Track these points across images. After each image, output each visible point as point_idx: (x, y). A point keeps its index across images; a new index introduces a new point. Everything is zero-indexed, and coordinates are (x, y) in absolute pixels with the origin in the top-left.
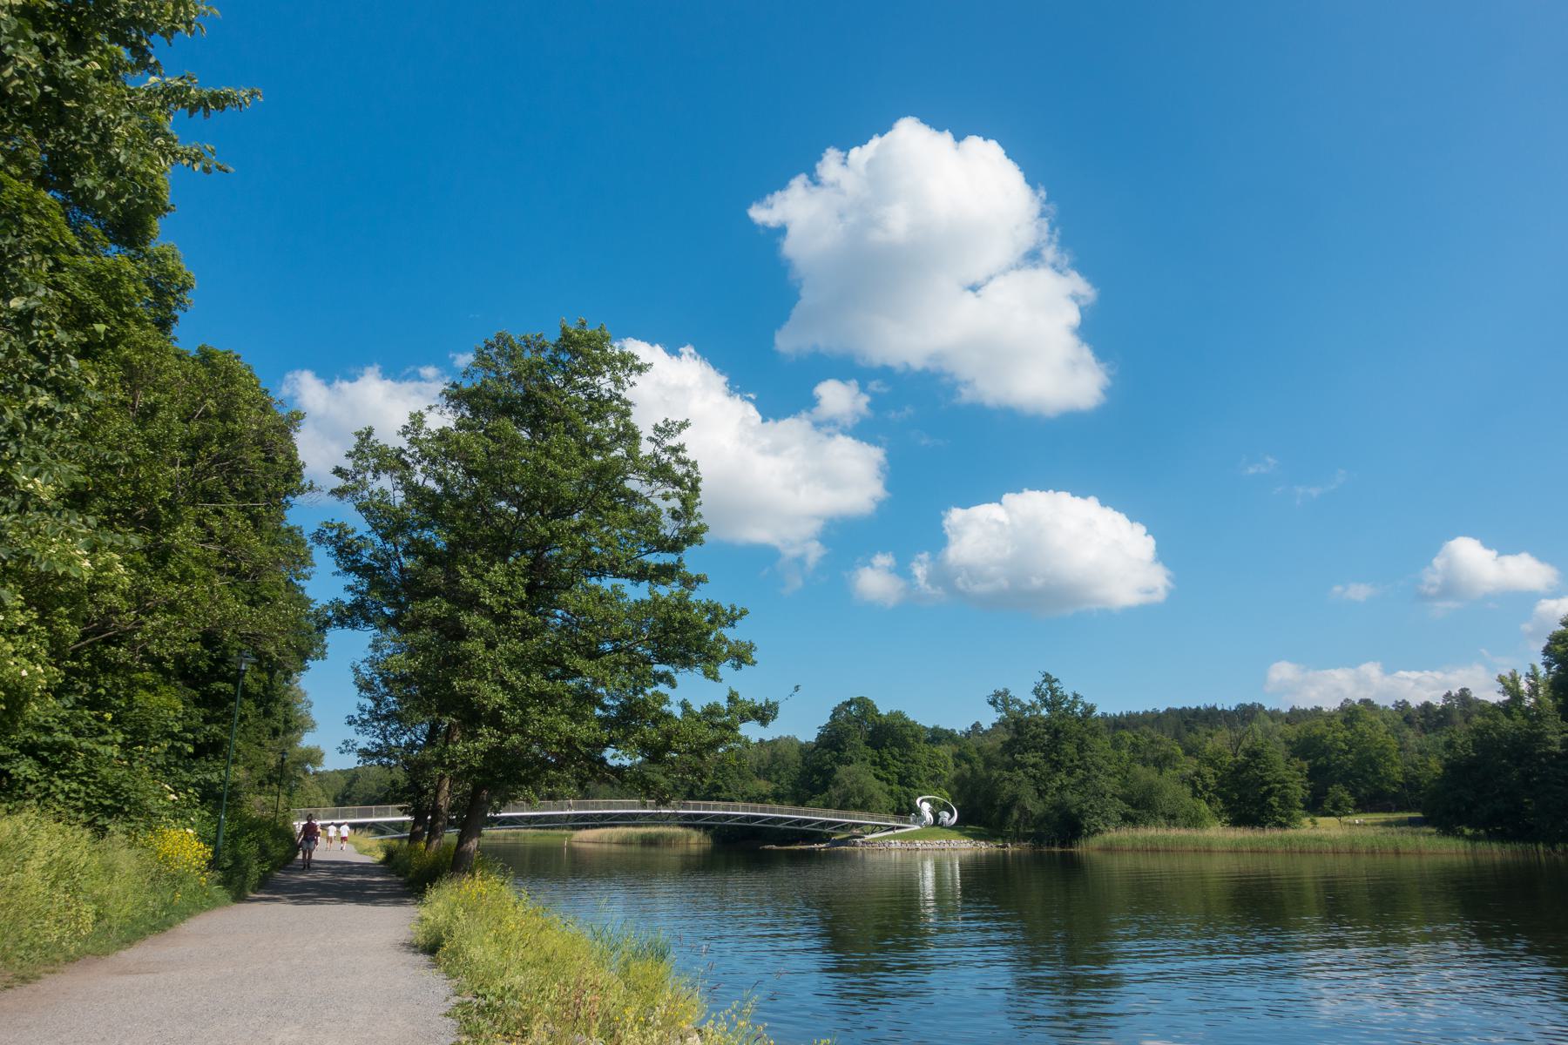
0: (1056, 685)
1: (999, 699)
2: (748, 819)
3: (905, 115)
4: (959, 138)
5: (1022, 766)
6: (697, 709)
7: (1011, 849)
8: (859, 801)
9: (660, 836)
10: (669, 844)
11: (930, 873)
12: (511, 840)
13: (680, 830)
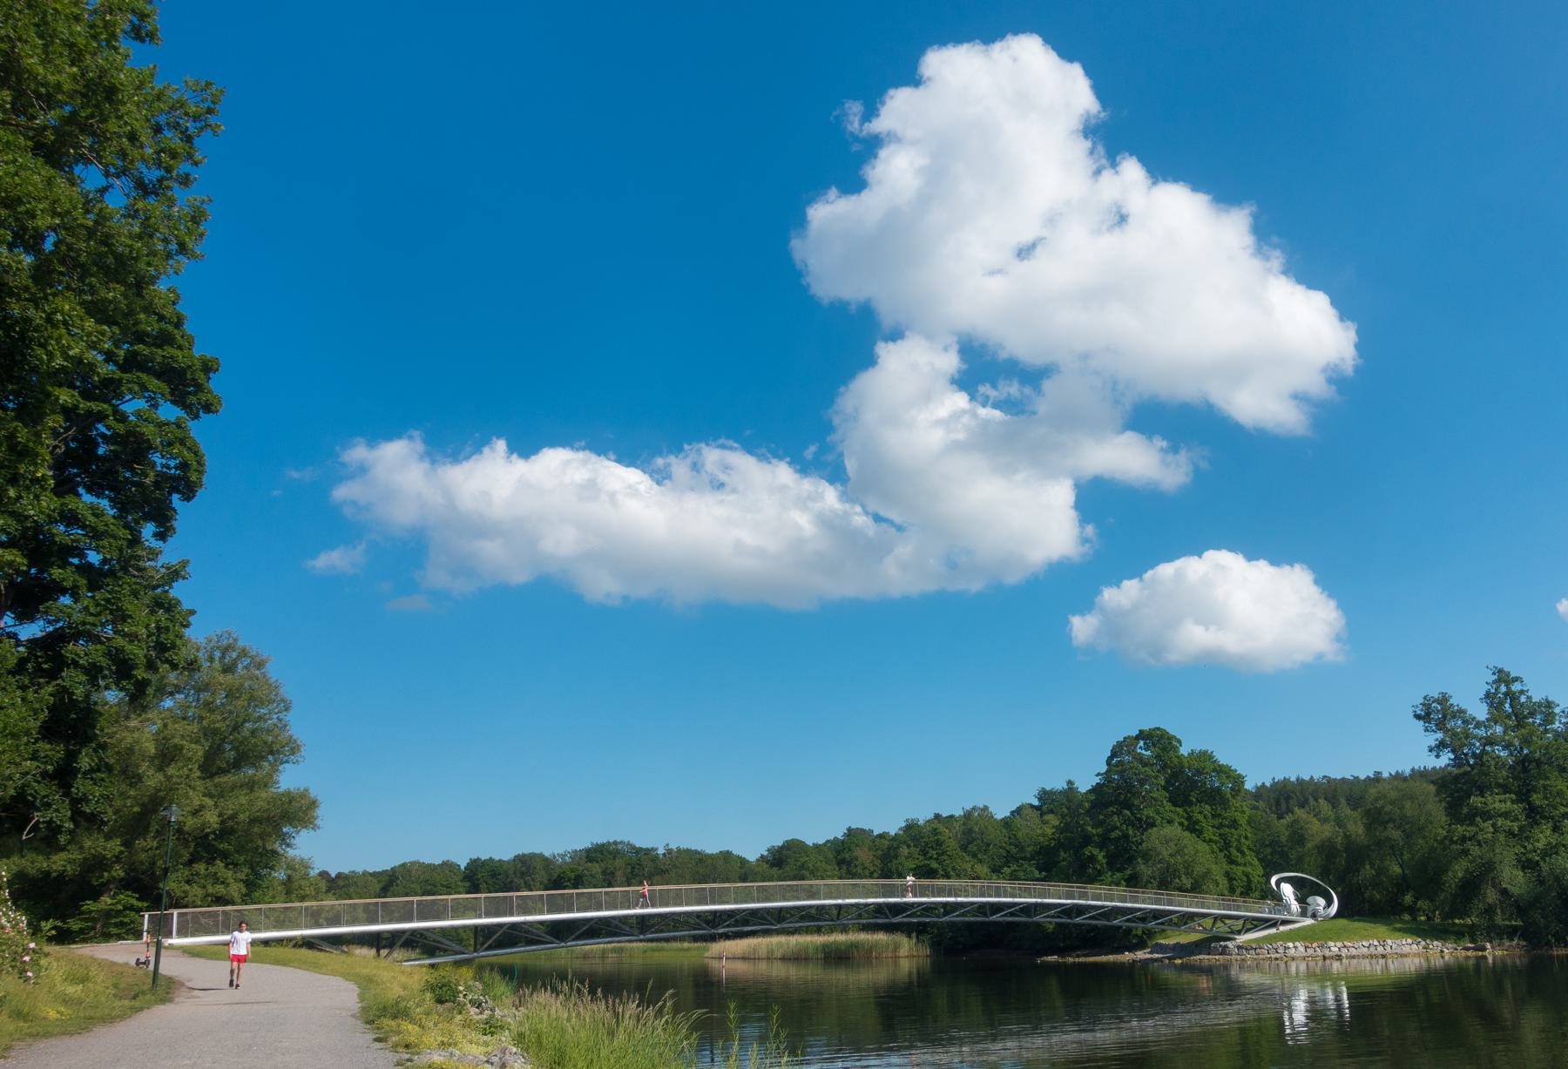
0: (1516, 687)
1: (1436, 713)
2: (982, 908)
3: (1326, 292)
5: (1486, 815)
6: (177, 591)
7: (1493, 952)
8: (1187, 883)
9: (855, 945)
12: (612, 958)
13: (881, 937)
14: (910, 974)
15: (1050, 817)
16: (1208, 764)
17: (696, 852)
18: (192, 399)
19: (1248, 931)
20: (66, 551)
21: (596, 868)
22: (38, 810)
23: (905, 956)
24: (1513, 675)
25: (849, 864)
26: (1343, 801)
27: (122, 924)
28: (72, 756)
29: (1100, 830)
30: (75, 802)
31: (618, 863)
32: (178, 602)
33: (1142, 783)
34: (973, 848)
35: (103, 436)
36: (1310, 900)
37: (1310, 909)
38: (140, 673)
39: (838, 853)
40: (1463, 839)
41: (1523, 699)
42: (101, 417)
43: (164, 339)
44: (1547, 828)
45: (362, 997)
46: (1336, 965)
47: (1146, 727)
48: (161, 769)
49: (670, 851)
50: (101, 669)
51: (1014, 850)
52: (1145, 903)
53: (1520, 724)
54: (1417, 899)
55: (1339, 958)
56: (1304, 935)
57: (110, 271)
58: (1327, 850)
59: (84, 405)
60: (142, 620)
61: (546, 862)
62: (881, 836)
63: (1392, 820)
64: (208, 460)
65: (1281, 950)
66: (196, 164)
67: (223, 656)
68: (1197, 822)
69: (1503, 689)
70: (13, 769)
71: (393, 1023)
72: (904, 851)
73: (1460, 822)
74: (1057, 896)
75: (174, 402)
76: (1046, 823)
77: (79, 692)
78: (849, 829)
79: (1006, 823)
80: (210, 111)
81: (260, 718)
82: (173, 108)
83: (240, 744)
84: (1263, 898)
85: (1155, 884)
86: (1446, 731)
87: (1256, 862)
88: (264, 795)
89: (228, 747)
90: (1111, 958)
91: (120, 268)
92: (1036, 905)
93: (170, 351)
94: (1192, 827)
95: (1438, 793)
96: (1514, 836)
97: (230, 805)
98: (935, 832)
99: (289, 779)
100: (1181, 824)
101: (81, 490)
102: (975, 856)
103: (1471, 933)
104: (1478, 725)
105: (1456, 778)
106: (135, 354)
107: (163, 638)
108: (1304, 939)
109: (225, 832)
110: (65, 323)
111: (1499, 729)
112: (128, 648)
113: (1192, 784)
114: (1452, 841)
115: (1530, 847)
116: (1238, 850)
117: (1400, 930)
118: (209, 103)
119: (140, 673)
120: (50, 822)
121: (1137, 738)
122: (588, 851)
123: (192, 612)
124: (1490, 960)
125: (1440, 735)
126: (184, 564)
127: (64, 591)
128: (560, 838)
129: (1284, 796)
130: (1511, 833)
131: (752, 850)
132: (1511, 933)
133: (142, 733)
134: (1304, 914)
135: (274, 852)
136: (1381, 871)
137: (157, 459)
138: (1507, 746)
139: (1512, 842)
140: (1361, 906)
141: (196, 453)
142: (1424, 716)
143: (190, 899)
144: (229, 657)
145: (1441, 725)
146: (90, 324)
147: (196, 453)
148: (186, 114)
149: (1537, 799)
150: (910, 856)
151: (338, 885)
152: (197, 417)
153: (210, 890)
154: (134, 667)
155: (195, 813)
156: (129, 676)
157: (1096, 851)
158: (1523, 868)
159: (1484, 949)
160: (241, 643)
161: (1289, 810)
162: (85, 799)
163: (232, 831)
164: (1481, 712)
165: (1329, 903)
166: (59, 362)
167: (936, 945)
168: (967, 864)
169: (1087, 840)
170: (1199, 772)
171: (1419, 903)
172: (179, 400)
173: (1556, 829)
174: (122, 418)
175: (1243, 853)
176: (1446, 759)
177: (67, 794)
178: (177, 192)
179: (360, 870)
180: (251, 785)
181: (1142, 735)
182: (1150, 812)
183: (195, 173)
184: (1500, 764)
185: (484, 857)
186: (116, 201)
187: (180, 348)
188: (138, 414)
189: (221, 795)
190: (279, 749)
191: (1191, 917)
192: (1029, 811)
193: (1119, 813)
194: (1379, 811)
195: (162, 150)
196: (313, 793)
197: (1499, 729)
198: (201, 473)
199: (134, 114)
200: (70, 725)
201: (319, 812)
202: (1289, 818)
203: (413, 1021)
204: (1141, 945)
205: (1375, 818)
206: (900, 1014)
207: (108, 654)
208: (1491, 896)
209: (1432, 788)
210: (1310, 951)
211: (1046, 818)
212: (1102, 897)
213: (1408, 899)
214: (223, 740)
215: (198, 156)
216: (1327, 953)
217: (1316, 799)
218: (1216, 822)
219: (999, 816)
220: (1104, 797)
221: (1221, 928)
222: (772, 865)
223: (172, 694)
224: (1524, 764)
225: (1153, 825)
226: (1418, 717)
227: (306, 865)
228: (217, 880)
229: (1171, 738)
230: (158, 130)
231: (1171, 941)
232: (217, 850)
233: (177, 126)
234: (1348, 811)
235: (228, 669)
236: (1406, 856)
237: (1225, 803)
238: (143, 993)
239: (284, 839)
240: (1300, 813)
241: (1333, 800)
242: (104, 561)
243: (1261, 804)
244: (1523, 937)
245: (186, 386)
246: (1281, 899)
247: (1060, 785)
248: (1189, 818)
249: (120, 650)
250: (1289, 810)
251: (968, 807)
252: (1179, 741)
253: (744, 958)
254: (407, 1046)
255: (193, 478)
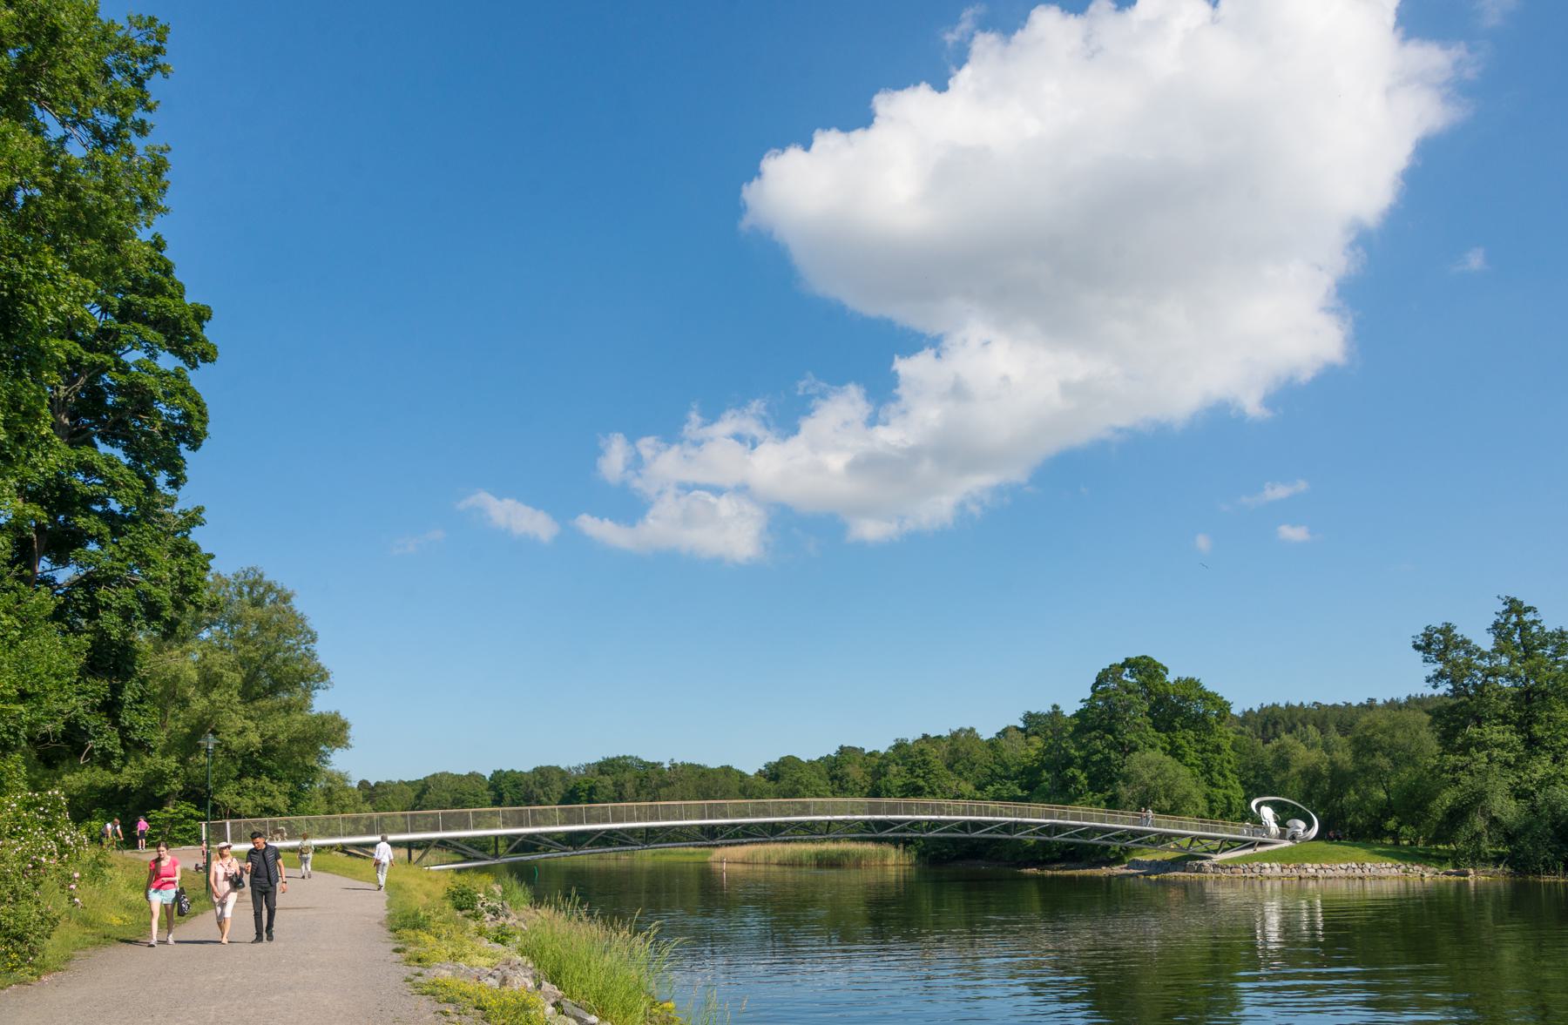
0: (1528, 617)
1: (1438, 644)
2: (963, 826)
4: (807, 146)
5: (1482, 745)
6: (196, 535)
7: (1475, 877)
8: (1167, 804)
9: (846, 854)
10: (858, 865)
11: (1274, 921)
13: (870, 847)
14: (897, 882)
15: (1034, 739)
16: (1194, 691)
17: (699, 767)
18: (188, 349)
19: (1225, 850)
20: (87, 501)
21: (608, 781)
22: (92, 738)
23: (894, 863)
24: (1526, 605)
25: (841, 779)
26: (1333, 727)
27: (185, 830)
28: (117, 690)
29: (1082, 753)
30: (123, 731)
31: (627, 775)
32: (197, 548)
33: (1127, 709)
34: (958, 767)
35: (109, 386)
36: (1289, 823)
37: (1289, 833)
38: (168, 613)
39: (831, 769)
40: (1455, 769)
41: (1534, 629)
42: (103, 369)
43: (156, 289)
44: (1547, 759)
45: (390, 905)
46: (1311, 884)
47: (1133, 655)
48: (205, 695)
49: (674, 766)
50: (133, 610)
51: (999, 770)
52: (1122, 822)
53: (1529, 654)
54: (1400, 824)
55: (1315, 878)
56: (1282, 857)
57: (83, 221)
58: (1312, 776)
59: (87, 357)
60: (165, 565)
61: (563, 774)
62: (871, 754)
63: (1382, 748)
64: (210, 409)
65: (1257, 870)
66: (149, 109)
67: (251, 592)
68: (1180, 747)
69: (1514, 619)
70: (60, 706)
71: (412, 933)
72: (893, 769)
73: (1454, 752)
74: (1036, 815)
75: (171, 351)
76: (1031, 744)
77: (115, 634)
78: (842, 748)
79: (992, 744)
80: (157, 50)
81: (289, 649)
82: (119, 48)
83: (275, 668)
84: (1243, 819)
85: (1134, 805)
86: (1447, 662)
87: (1238, 785)
88: (299, 717)
89: (264, 675)
90: (1088, 872)
91: (85, 222)
92: (1016, 824)
93: (161, 300)
94: (1175, 752)
95: (1432, 723)
96: (1510, 766)
97: (269, 728)
98: (922, 752)
99: (322, 703)
100: (1163, 749)
101: (97, 440)
102: (960, 774)
103: (1455, 858)
104: (1482, 656)
105: (1453, 709)
106: (129, 303)
107: (186, 580)
108: (1281, 860)
109: (267, 751)
110: (51, 279)
111: (1504, 660)
112: (155, 591)
113: (1178, 711)
114: (1443, 771)
115: (1526, 777)
116: (1220, 774)
117: (1379, 853)
118: (154, 42)
119: (168, 613)
120: (103, 749)
121: (1123, 666)
122: (600, 764)
123: (211, 556)
124: (1472, 883)
125: (1439, 666)
126: (199, 510)
127: (91, 537)
128: (575, 752)
129: (1271, 721)
130: (1507, 764)
131: (751, 764)
132: (1498, 859)
133: (183, 663)
134: (1282, 836)
135: (314, 769)
136: (1365, 797)
137: (162, 407)
138: (1513, 677)
139: (1507, 772)
140: (1339, 829)
141: (197, 403)
142: (1425, 645)
143: (241, 809)
144: (257, 591)
145: (1441, 656)
146: (74, 279)
147: (197, 403)
148: (133, 55)
149: (1537, 730)
150: (899, 774)
151: (373, 794)
152: (195, 366)
153: (259, 801)
154: (162, 609)
155: (240, 733)
156: (158, 618)
157: (1078, 772)
158: (1517, 797)
159: (1467, 874)
160: (266, 579)
161: (1276, 735)
162: (132, 727)
163: (274, 749)
164: (1486, 643)
165: (1310, 825)
166: (50, 318)
167: (921, 854)
168: (952, 782)
169: (1070, 762)
170: (1184, 699)
171: (1403, 828)
172: (178, 352)
173: (1555, 760)
174: (124, 369)
175: (1224, 777)
176: (1444, 688)
177: (116, 723)
178: (136, 141)
179: (396, 780)
180: (288, 709)
181: (1128, 663)
182: (1133, 737)
183: (148, 118)
184: (1502, 696)
185: (506, 769)
186: (77, 150)
187: (171, 296)
188: (138, 364)
189: (262, 718)
190: (313, 677)
191: (1169, 836)
192: (1014, 733)
193: (1102, 738)
194: (1368, 740)
195: (114, 97)
196: (344, 715)
197: (1504, 660)
198: (205, 423)
199: (83, 61)
200: (109, 661)
201: (351, 732)
202: (1275, 743)
203: (429, 932)
204: (1118, 860)
205: (1364, 747)
206: (889, 919)
207: (138, 597)
208: (1480, 823)
209: (1428, 718)
210: (1286, 872)
211: (1031, 739)
212: (1083, 817)
213: (1391, 824)
214: (258, 669)
215: (151, 101)
216: (1303, 874)
217: (1304, 725)
218: (1199, 747)
219: (985, 737)
220: (1085, 721)
221: (1198, 848)
222: (770, 779)
223: (208, 626)
224: (1527, 697)
225: (1135, 749)
226: (1417, 647)
227: (344, 778)
228: (264, 792)
229: (1157, 666)
230: (107, 72)
231: (1147, 858)
232: (262, 767)
233: (126, 69)
234: (1338, 737)
235: (257, 603)
236: (1393, 783)
237: (1209, 730)
238: (199, 898)
239: (322, 757)
240: (1287, 738)
241: (1322, 727)
242: (125, 509)
243: (1247, 729)
244: (1510, 863)
245: (182, 334)
246: (1260, 822)
247: (1046, 709)
248: (1172, 743)
249: (147, 594)
250: (1276, 735)
251: (955, 729)
252: (1166, 670)
253: (743, 863)
254: (419, 960)
255: (197, 428)
